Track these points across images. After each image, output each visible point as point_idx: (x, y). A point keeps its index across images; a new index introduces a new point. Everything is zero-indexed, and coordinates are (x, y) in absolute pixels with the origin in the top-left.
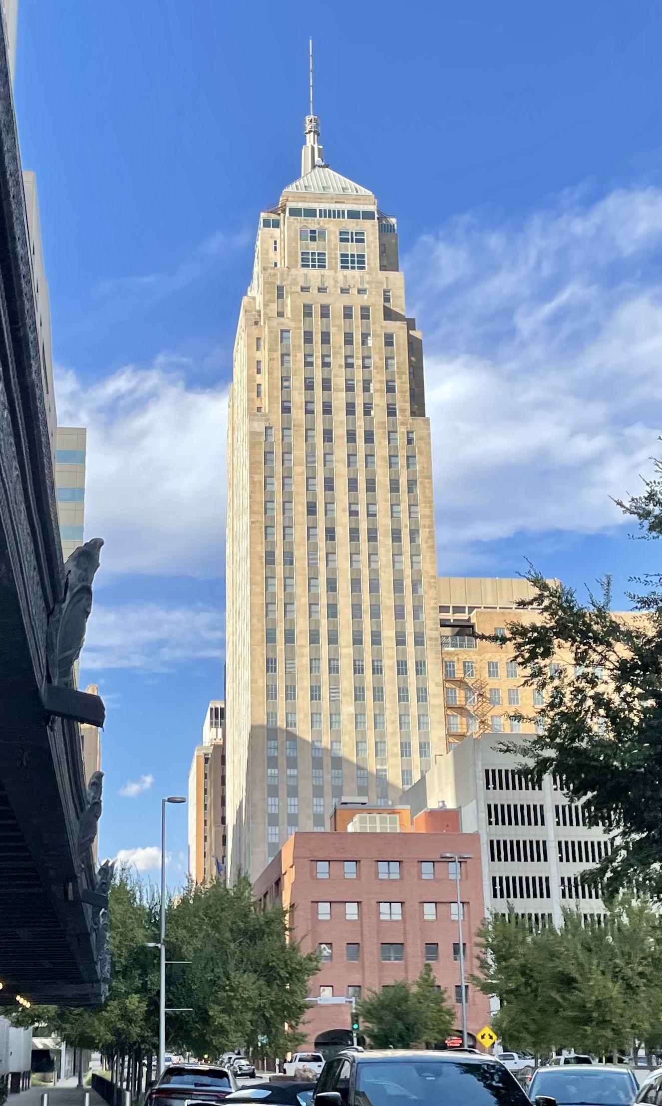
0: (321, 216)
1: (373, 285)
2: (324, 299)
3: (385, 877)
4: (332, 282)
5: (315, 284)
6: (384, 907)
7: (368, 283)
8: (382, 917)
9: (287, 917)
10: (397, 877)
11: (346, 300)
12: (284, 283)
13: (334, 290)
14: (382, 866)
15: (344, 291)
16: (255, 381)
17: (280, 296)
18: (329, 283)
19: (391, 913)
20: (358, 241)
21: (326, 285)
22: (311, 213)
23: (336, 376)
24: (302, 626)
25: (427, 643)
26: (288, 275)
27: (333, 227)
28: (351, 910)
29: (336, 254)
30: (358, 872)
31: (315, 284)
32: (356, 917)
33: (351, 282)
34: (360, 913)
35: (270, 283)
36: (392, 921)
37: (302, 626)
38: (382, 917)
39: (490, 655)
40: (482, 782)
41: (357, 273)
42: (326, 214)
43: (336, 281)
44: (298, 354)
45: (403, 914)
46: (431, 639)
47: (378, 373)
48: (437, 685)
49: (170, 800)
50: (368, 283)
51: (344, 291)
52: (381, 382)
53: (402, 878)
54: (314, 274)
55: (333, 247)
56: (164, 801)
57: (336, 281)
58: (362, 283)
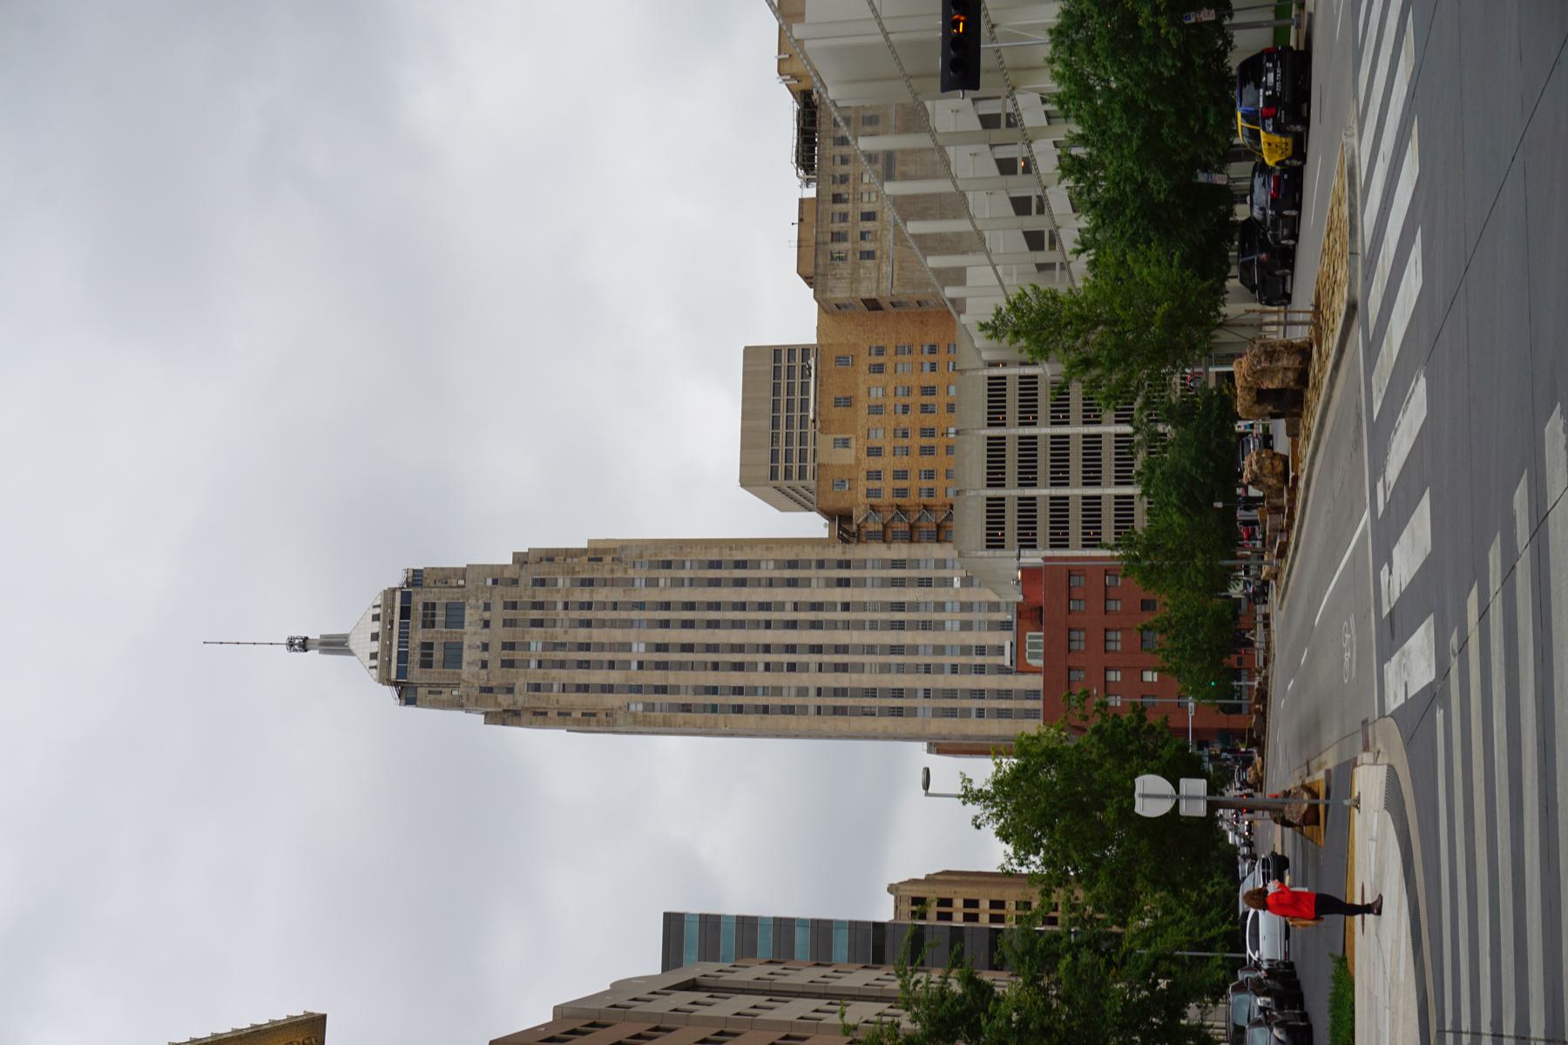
2: (496, 646)
6: (1111, 646)
11: (497, 624)
14: (1074, 646)
15: (487, 624)
18: (478, 641)
19: (1116, 642)
22: (403, 657)
24: (597, 635)
27: (418, 636)
28: (1114, 676)
30: (1079, 669)
33: (477, 617)
36: (1122, 641)
37: (597, 635)
40: (999, 552)
41: (468, 612)
42: (404, 642)
49: (926, 785)
51: (487, 624)
54: (468, 656)
56: (927, 794)
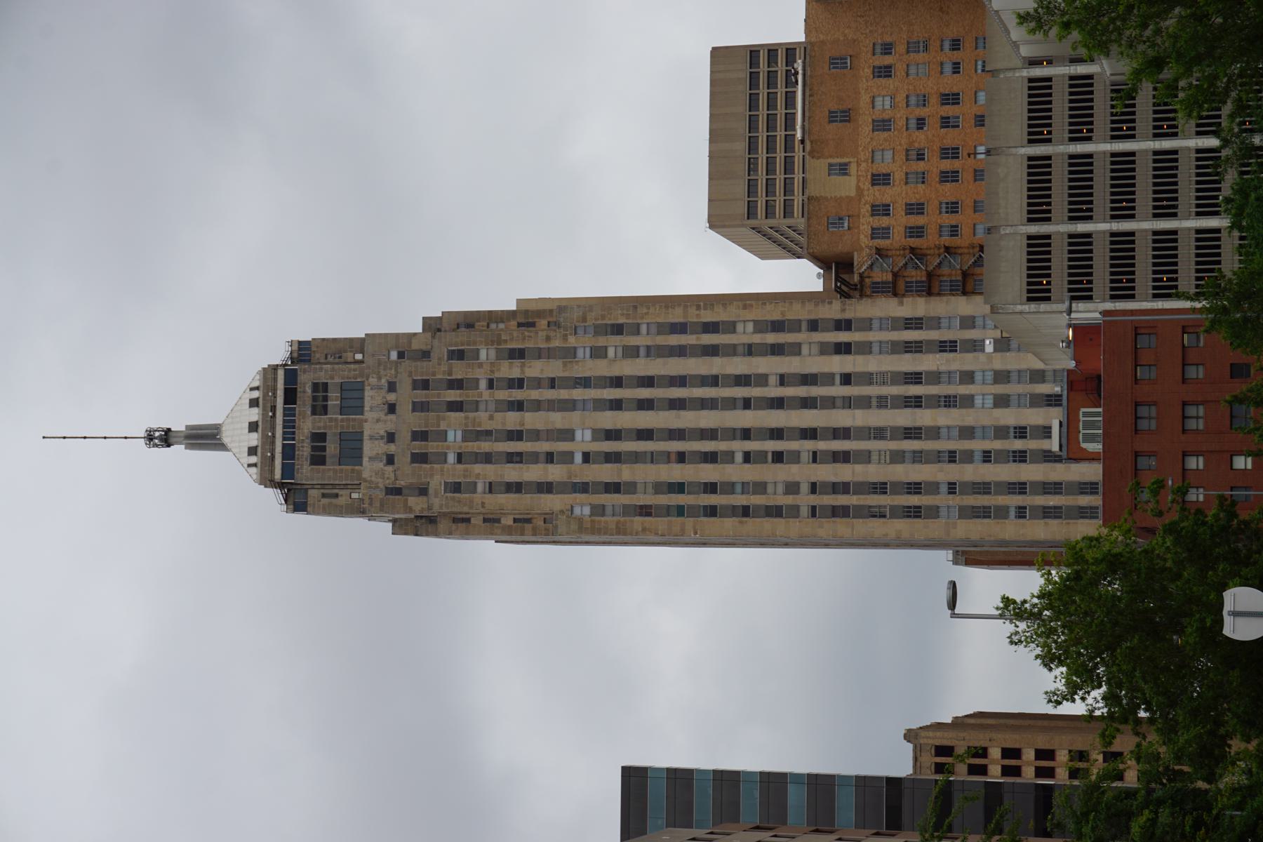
0: (293, 439)
1: (382, 372)
2: (404, 436)
3: (1153, 423)
4: (380, 425)
5: (382, 448)
6: (1191, 425)
7: (380, 378)
8: (1201, 427)
9: (1226, 190)
10: (1153, 409)
11: (405, 408)
12: (381, 486)
13: (390, 423)
14: (1143, 425)
15: (392, 409)
16: (510, 527)
17: (397, 491)
18: (381, 430)
20: (326, 390)
21: (382, 433)
23: (504, 424)
25: (848, 315)
26: (371, 482)
27: (307, 425)
28: (1194, 463)
29: (342, 420)
30: (1150, 454)
31: (382, 448)
32: (1201, 459)
33: (379, 400)
34: (1197, 454)
35: (382, 505)
38: (1201, 427)
39: (862, 236)
40: (1043, 306)
43: (378, 420)
44: (477, 471)
45: (1197, 404)
46: (843, 310)
47: (499, 370)
48: (901, 303)
50: (380, 378)
51: (392, 409)
52: (510, 367)
53: (1155, 403)
55: (332, 423)
57: (378, 420)
58: (380, 388)
